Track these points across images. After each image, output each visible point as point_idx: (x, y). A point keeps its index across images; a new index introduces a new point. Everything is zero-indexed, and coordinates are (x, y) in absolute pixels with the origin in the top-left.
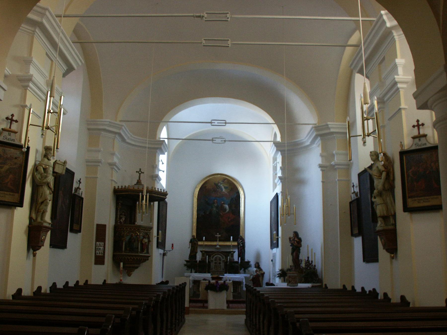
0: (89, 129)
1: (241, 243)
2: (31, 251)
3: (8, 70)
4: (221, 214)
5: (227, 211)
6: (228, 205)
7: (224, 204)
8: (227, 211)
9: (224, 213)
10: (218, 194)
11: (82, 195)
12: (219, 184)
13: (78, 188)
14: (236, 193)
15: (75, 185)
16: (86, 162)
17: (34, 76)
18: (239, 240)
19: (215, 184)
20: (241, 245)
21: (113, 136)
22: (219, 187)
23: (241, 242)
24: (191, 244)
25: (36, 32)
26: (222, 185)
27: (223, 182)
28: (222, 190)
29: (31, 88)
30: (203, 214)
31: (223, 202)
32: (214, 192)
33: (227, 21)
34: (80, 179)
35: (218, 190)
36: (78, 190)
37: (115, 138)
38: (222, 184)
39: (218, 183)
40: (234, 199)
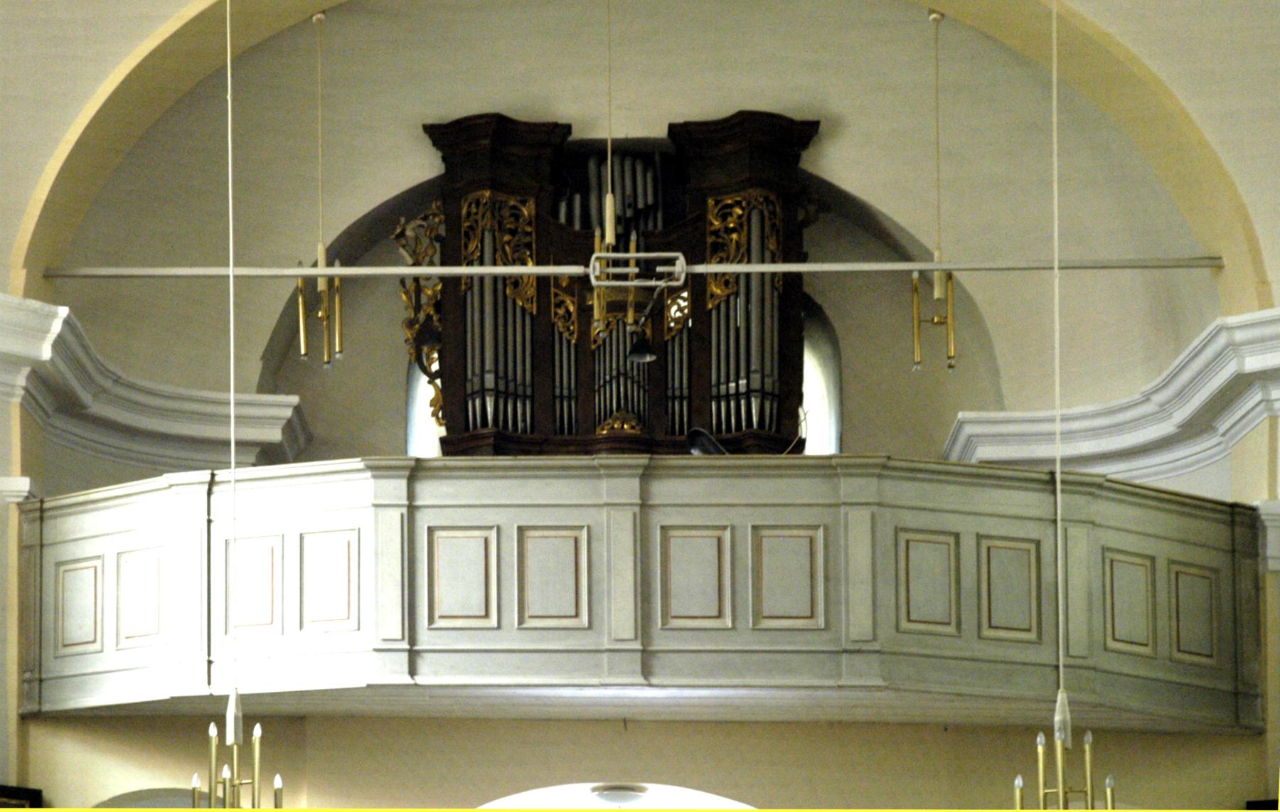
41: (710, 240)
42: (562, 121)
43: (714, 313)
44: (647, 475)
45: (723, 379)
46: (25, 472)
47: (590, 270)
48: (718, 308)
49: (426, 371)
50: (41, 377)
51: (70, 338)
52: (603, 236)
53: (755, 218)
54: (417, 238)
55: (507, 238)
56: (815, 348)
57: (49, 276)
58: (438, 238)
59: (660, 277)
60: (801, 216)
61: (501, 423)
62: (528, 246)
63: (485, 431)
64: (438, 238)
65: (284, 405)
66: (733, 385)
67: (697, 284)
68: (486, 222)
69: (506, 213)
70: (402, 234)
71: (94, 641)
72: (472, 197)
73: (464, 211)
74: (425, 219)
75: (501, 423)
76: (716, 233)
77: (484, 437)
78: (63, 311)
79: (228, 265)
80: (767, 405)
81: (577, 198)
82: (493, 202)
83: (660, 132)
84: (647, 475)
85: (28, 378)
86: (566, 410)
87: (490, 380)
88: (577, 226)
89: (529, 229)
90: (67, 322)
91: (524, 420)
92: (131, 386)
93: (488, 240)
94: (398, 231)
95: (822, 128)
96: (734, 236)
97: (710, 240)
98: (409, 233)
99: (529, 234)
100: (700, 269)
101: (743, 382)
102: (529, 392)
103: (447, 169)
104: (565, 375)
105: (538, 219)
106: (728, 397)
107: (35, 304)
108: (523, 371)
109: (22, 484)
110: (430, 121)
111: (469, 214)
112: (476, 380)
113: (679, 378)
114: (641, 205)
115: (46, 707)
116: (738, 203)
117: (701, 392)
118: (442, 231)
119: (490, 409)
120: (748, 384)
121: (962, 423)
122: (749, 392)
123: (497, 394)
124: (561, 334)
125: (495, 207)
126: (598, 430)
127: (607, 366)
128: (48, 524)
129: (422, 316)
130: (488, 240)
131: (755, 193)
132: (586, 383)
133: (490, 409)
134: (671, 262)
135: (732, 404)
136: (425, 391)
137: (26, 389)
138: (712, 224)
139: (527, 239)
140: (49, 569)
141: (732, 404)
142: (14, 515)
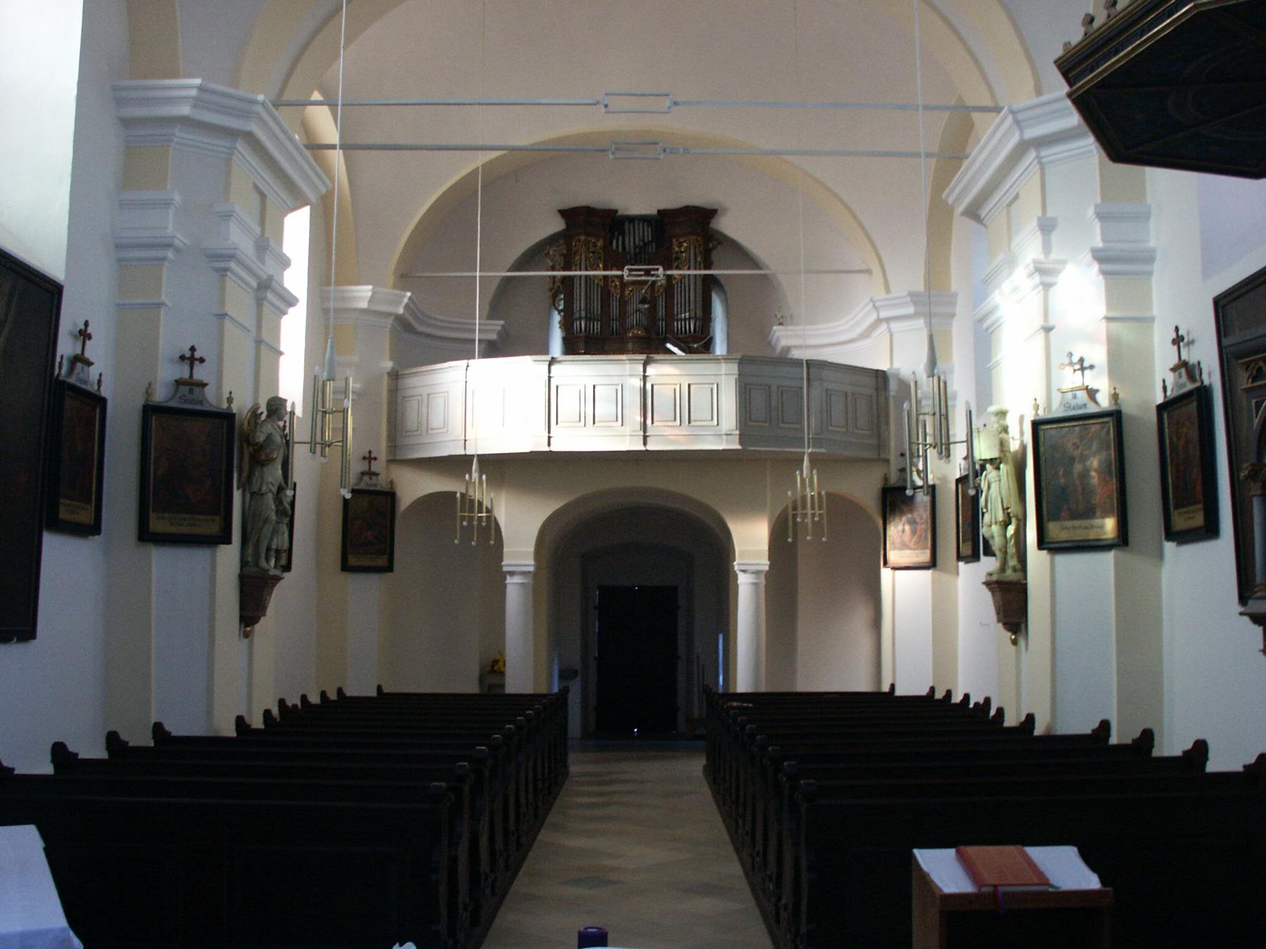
0: (127, 123)
2: (243, 626)
3: (181, 238)
11: (102, 388)
13: (80, 360)
15: (66, 347)
16: (117, 247)
17: (275, 278)
21: (228, 144)
25: (238, 150)
29: (234, 273)
33: (659, 159)
34: (86, 324)
36: (79, 365)
37: (233, 154)
41: (674, 256)
42: (613, 208)
43: (676, 286)
44: (646, 364)
45: (679, 312)
46: (391, 359)
47: (624, 273)
48: (677, 284)
49: (557, 310)
50: (400, 320)
51: (411, 305)
52: (585, 690)
53: (692, 247)
54: (554, 256)
55: (591, 255)
56: (717, 293)
57: (403, 276)
58: (563, 255)
59: (653, 275)
60: (711, 245)
61: (588, 331)
62: (600, 258)
63: (581, 335)
64: (563, 255)
65: (498, 324)
66: (683, 315)
67: (669, 278)
68: (584, 249)
69: (591, 245)
70: (548, 253)
71: (418, 430)
72: (577, 238)
73: (574, 244)
74: (558, 247)
75: (588, 331)
76: (677, 253)
77: (580, 337)
78: (409, 294)
79: (476, 271)
80: (698, 323)
81: (620, 238)
82: (586, 240)
83: (654, 212)
84: (646, 364)
85: (394, 320)
86: (615, 325)
87: (583, 314)
88: (620, 250)
89: (600, 251)
90: (410, 298)
91: (597, 329)
92: (435, 319)
93: (583, 257)
94: (546, 252)
95: (719, 211)
96: (684, 255)
97: (674, 256)
98: (551, 253)
99: (600, 253)
100: (669, 272)
101: (687, 314)
102: (599, 318)
103: (567, 227)
104: (615, 311)
105: (604, 247)
106: (681, 320)
107: (397, 292)
108: (597, 307)
109: (388, 365)
110: (560, 208)
111: (576, 245)
112: (578, 314)
113: (661, 312)
114: (646, 241)
115: (398, 458)
116: (685, 241)
117: (670, 316)
118: (565, 251)
119: (583, 326)
120: (689, 315)
121: (775, 331)
122: (689, 319)
123: (587, 318)
124: (613, 295)
125: (587, 243)
126: (628, 334)
127: (631, 308)
128: (400, 381)
129: (556, 288)
130: (583, 257)
131: (693, 237)
132: (623, 314)
133: (583, 326)
134: (658, 269)
135: (683, 323)
136: (557, 318)
137: (392, 325)
138: (674, 249)
139: (599, 256)
140: (399, 399)
141: (683, 323)
142: (386, 378)
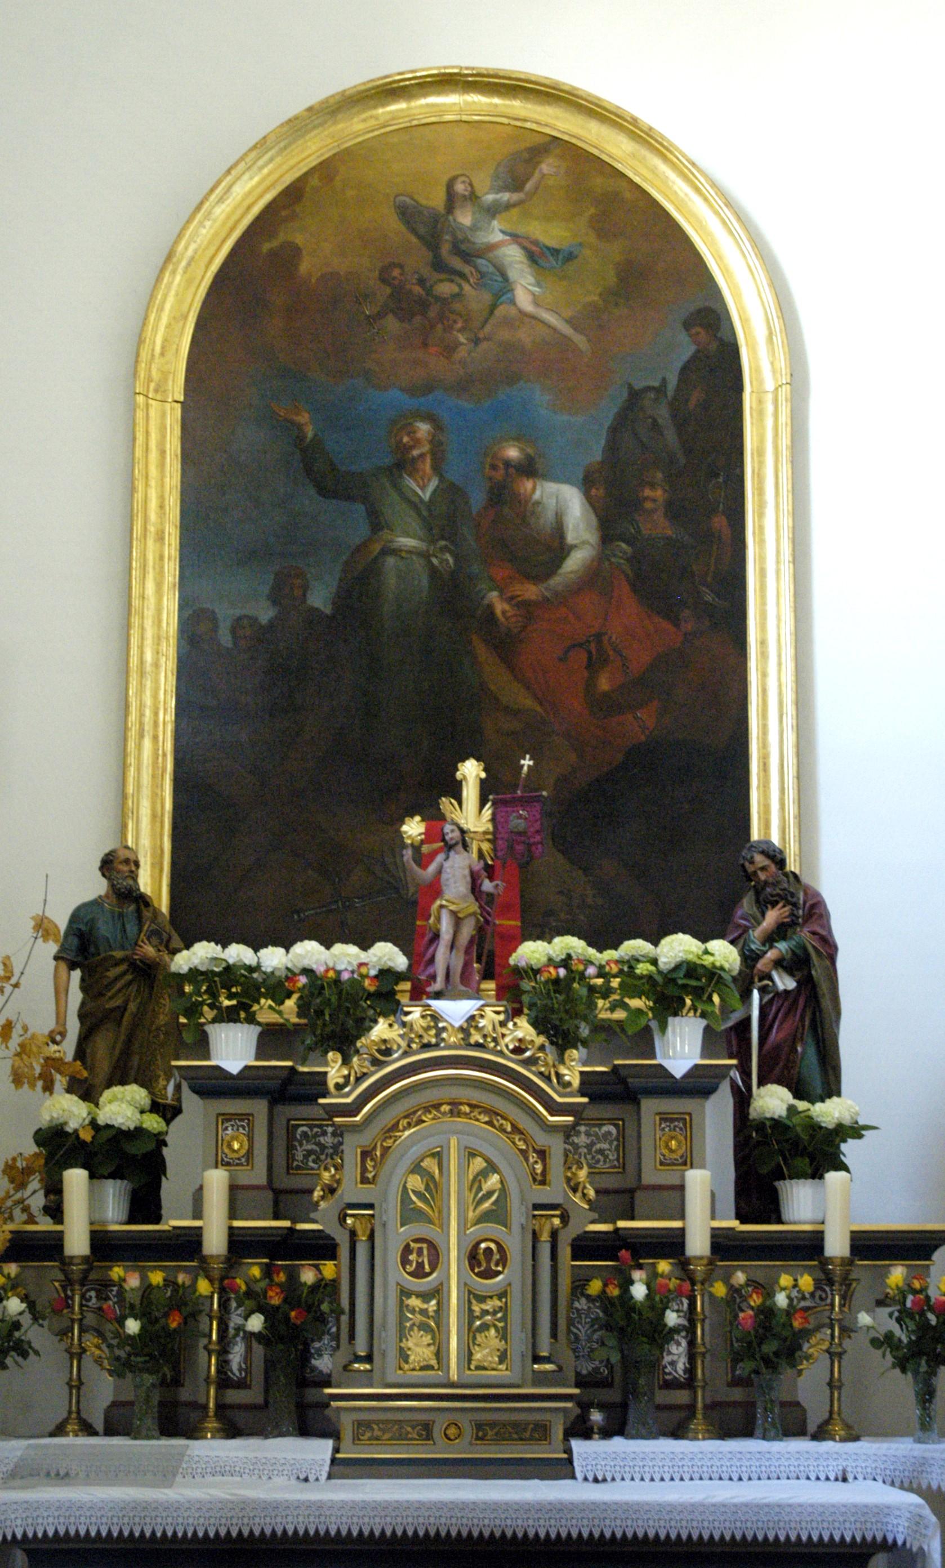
1: (782, 946)
4: (500, 607)
5: (575, 562)
6: (587, 484)
7: (529, 469)
8: (575, 562)
9: (531, 591)
10: (449, 349)
12: (465, 218)
14: (687, 325)
18: (747, 904)
19: (407, 213)
20: (784, 982)
22: (467, 252)
23: (770, 939)
24: (85, 987)
26: (494, 233)
27: (516, 184)
28: (504, 288)
30: (265, 614)
31: (513, 453)
32: (392, 324)
35: (445, 289)
38: (493, 211)
39: (452, 200)
40: (663, 413)
